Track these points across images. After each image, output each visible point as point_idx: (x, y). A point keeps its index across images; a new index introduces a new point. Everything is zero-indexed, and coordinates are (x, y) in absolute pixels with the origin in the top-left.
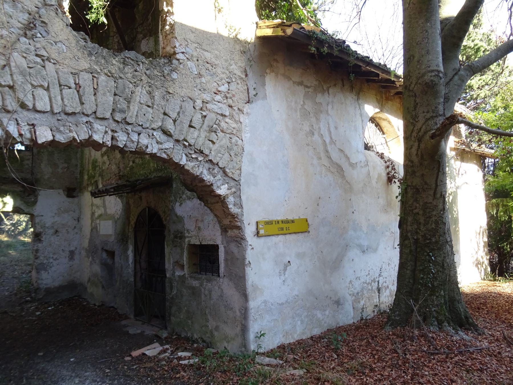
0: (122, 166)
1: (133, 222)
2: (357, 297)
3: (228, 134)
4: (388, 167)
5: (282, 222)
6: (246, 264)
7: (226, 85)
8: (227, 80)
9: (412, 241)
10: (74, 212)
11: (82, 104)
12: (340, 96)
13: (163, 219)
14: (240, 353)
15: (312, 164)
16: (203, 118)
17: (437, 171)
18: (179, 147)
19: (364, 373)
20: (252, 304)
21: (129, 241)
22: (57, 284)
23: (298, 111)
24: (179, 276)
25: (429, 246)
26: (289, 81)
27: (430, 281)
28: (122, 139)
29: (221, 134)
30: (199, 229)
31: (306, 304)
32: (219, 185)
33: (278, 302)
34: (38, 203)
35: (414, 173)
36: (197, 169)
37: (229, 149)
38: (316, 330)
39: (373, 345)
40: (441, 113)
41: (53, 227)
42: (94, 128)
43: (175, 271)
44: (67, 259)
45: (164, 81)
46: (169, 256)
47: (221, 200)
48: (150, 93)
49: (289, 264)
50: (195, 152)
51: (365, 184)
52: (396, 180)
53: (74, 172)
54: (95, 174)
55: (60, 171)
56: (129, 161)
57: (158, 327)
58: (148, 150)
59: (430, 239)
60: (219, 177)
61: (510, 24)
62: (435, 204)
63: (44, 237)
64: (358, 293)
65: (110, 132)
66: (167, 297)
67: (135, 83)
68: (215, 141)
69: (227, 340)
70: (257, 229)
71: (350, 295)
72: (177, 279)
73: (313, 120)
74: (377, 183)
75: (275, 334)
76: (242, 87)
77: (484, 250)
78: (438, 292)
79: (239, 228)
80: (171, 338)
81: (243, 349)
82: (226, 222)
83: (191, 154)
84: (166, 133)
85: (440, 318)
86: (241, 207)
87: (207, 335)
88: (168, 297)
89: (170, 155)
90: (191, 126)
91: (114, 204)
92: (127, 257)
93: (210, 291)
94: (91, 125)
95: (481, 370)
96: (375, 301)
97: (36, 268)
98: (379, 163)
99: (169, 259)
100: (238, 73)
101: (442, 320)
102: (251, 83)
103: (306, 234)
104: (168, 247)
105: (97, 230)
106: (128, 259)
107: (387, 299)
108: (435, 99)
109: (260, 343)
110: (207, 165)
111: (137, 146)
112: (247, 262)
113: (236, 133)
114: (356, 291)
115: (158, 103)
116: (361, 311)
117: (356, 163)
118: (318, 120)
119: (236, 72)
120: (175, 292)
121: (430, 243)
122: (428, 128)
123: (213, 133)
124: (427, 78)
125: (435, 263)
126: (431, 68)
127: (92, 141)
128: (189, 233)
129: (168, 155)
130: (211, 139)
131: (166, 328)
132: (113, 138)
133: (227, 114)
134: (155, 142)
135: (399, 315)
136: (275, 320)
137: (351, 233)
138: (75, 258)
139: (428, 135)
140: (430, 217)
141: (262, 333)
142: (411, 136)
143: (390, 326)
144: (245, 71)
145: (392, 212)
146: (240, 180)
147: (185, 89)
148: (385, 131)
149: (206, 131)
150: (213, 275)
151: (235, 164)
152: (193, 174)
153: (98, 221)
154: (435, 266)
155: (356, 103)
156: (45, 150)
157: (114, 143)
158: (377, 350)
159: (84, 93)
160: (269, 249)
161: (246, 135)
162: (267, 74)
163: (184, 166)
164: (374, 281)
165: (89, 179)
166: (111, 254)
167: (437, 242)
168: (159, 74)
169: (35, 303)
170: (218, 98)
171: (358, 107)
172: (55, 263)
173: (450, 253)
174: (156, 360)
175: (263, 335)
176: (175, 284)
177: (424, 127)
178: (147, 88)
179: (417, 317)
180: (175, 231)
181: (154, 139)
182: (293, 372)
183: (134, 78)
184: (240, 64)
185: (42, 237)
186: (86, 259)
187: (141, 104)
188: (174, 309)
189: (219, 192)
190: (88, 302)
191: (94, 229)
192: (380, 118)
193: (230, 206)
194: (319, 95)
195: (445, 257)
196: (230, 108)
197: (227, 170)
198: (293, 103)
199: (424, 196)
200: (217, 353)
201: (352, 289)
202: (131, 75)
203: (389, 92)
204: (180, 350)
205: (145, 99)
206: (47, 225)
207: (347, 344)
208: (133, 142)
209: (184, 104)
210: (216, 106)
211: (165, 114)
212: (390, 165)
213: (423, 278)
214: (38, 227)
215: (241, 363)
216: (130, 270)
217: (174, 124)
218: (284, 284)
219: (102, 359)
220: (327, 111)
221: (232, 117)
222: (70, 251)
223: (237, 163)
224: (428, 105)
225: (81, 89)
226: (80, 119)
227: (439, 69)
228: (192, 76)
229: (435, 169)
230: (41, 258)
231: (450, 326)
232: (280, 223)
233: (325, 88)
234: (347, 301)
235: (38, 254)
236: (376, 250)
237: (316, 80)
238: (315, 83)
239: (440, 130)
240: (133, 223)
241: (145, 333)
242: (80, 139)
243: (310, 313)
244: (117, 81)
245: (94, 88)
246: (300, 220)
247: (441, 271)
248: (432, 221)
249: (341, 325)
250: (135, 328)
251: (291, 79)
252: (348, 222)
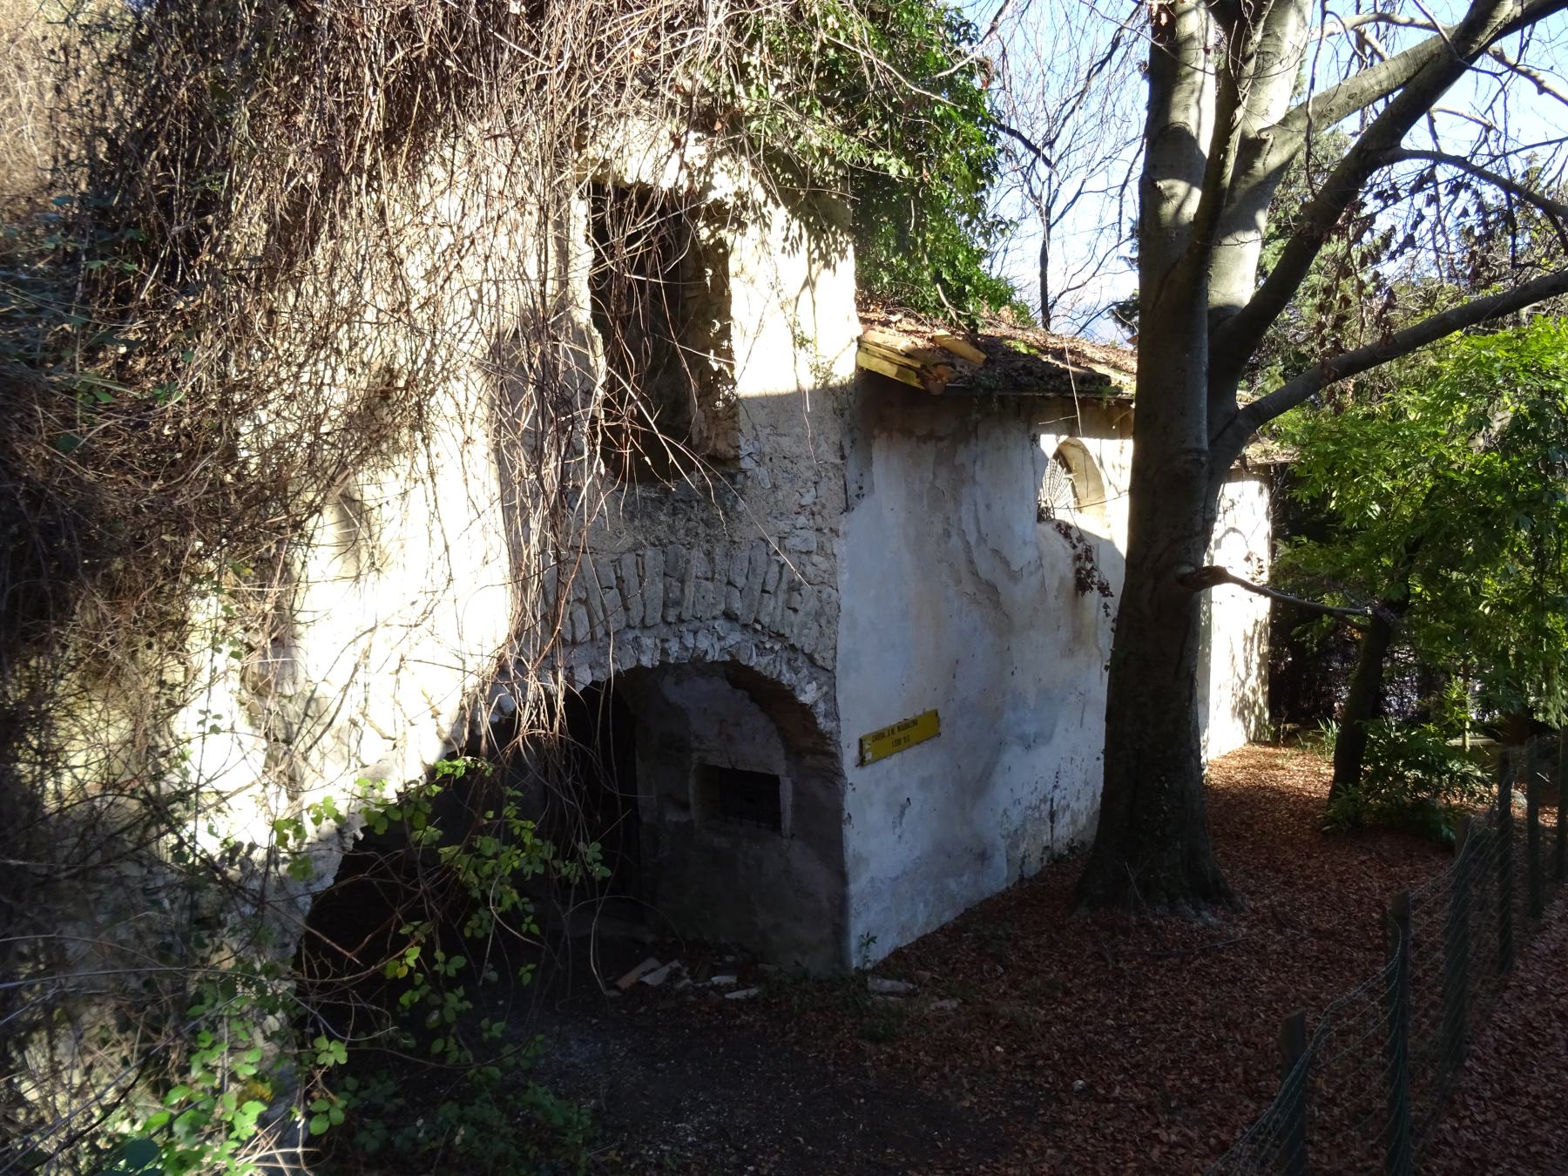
2: (1014, 838)
19: (1055, 1000)
20: (854, 888)
81: (837, 966)
90: (764, 591)
95: (1233, 981)
102: (852, 472)
112: (845, 816)
113: (827, 581)
114: (1012, 829)
126: (1186, 445)
144: (841, 448)
158: (1070, 955)
164: (1044, 801)
175: (873, 940)
182: (941, 1004)
189: (803, 699)
197: (816, 656)
208: (687, 649)
211: (729, 583)
212: (1083, 548)
215: (842, 989)
249: (987, 895)
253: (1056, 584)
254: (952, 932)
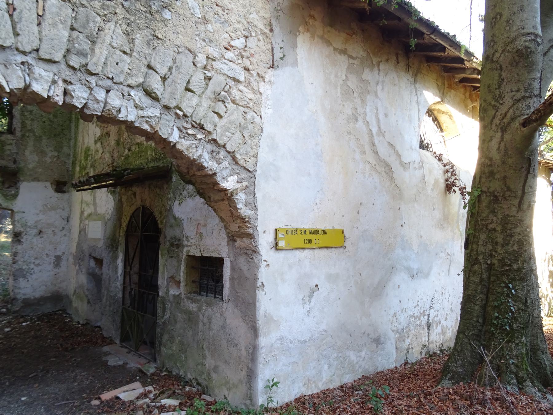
0: (116, 155)
1: (125, 224)
2: (402, 334)
3: (242, 106)
4: (447, 171)
5: (310, 231)
6: (258, 286)
7: (243, 40)
8: (244, 33)
9: (484, 266)
10: (63, 210)
11: (16, 34)
12: (393, 75)
13: (159, 222)
14: (243, 407)
15: (353, 159)
16: (207, 81)
17: (525, 173)
18: (169, 117)
20: (263, 341)
21: (120, 248)
22: (38, 294)
23: (339, 88)
24: (174, 296)
25: (509, 275)
26: (328, 46)
27: (508, 322)
28: (80, 96)
29: (231, 106)
30: (201, 236)
31: (336, 343)
32: (225, 175)
33: (300, 339)
34: (19, 197)
35: (492, 174)
36: (194, 150)
37: (242, 127)
38: (348, 376)
39: (427, 407)
40: (536, 92)
41: (36, 226)
42: (33, 73)
43: (170, 289)
44: (52, 265)
45: (151, 20)
46: (164, 268)
47: (227, 197)
48: (129, 34)
49: (316, 288)
50: (193, 126)
51: (418, 191)
52: (457, 189)
53: (65, 162)
54: (87, 165)
55: (48, 160)
56: (125, 148)
57: (146, 358)
58: (120, 116)
59: (510, 265)
60: (225, 164)
62: (519, 218)
63: (25, 237)
64: (403, 329)
65: (60, 83)
66: (158, 321)
67: (105, 15)
68: (222, 114)
69: (227, 386)
70: (276, 239)
71: (393, 331)
72: (171, 299)
73: (358, 101)
74: (432, 190)
75: (293, 382)
76: (264, 45)
77: (549, 281)
78: (517, 338)
79: (250, 236)
80: (159, 375)
81: (248, 402)
82: (234, 227)
83: (186, 128)
84: (149, 94)
85: (520, 374)
86: (255, 208)
87: (203, 377)
88: (160, 321)
89: (154, 126)
90: (188, 89)
91: (104, 201)
92: (116, 267)
93: (210, 320)
94: (29, 69)
96: (424, 339)
97: (13, 274)
98: (437, 166)
99: (163, 272)
100: (261, 26)
101: (523, 377)
103: (341, 249)
104: (162, 258)
105: (85, 233)
106: (116, 271)
107: (452, 345)
108: (529, 73)
109: (272, 395)
110: (209, 147)
111: (104, 108)
112: (259, 284)
114: (400, 327)
115: (139, 50)
116: (405, 352)
117: (409, 163)
118: (363, 101)
119: (256, 23)
120: (168, 316)
121: (510, 270)
122: (518, 113)
123: (220, 103)
124: (520, 43)
125: (516, 298)
126: (526, 31)
127: (31, 92)
128: (188, 241)
129: (151, 126)
130: (216, 111)
131: (155, 360)
132: (65, 93)
133: (242, 79)
134: (133, 106)
135: (462, 366)
136: (293, 363)
137: (399, 251)
138: (62, 265)
139: (517, 121)
140: (511, 236)
141: (275, 381)
142: (492, 124)
143: (449, 380)
144: (270, 24)
145: (449, 229)
146: (256, 171)
147: (182, 35)
148: (444, 127)
149: (210, 98)
150: (215, 297)
151: (249, 149)
152: (189, 158)
153: (87, 222)
154: (516, 302)
155: (413, 86)
156: (32, 134)
157: (68, 100)
159: (20, 19)
160: (290, 267)
161: (267, 111)
162: (300, 33)
163: (175, 145)
164: (423, 314)
165: (80, 170)
166: (99, 262)
167: (519, 270)
168: (144, 9)
169: (9, 316)
170: (229, 55)
171: (414, 91)
172: (36, 269)
173: (535, 286)
174: (132, 407)
176: (168, 305)
177: (511, 111)
178: (124, 26)
179: (489, 371)
180: (171, 238)
181: (131, 101)
183: (104, 9)
184: (262, 13)
185: (22, 238)
186: (73, 266)
187: (113, 48)
188: (166, 337)
190: (71, 318)
191: (83, 231)
192: (439, 111)
193: (239, 206)
194: (367, 71)
195: (529, 291)
196: (246, 72)
197: (238, 156)
198: (332, 77)
199: (505, 206)
200: (214, 403)
201: (396, 324)
202: (100, 4)
203: (454, 77)
204: (165, 395)
205: (120, 40)
206: (29, 224)
207: (390, 403)
209: (179, 57)
210: (226, 66)
211: (149, 67)
212: (450, 171)
213: (497, 317)
214: (18, 225)
216: (118, 284)
217: (164, 83)
218: (308, 315)
219: (63, 401)
220: (376, 93)
221: (248, 84)
222: (55, 257)
223: (252, 148)
224: (519, 81)
225: (15, 13)
226: (12, 58)
227: (536, 32)
228: (193, 20)
229: (523, 169)
230: (20, 263)
231: (534, 386)
232: (308, 233)
233: (374, 63)
234: (390, 340)
235: (17, 258)
236: (427, 275)
237: (364, 51)
238: (362, 53)
239: (540, 112)
240: (124, 225)
241: (128, 366)
242: (11, 87)
243: (340, 355)
244: (76, 9)
245: (38, 15)
246: (334, 230)
247: (522, 310)
248: (515, 241)
249: (380, 370)
250: (116, 357)
251: (332, 45)
252: (395, 237)
253: (433, 182)
254: (347, 390)
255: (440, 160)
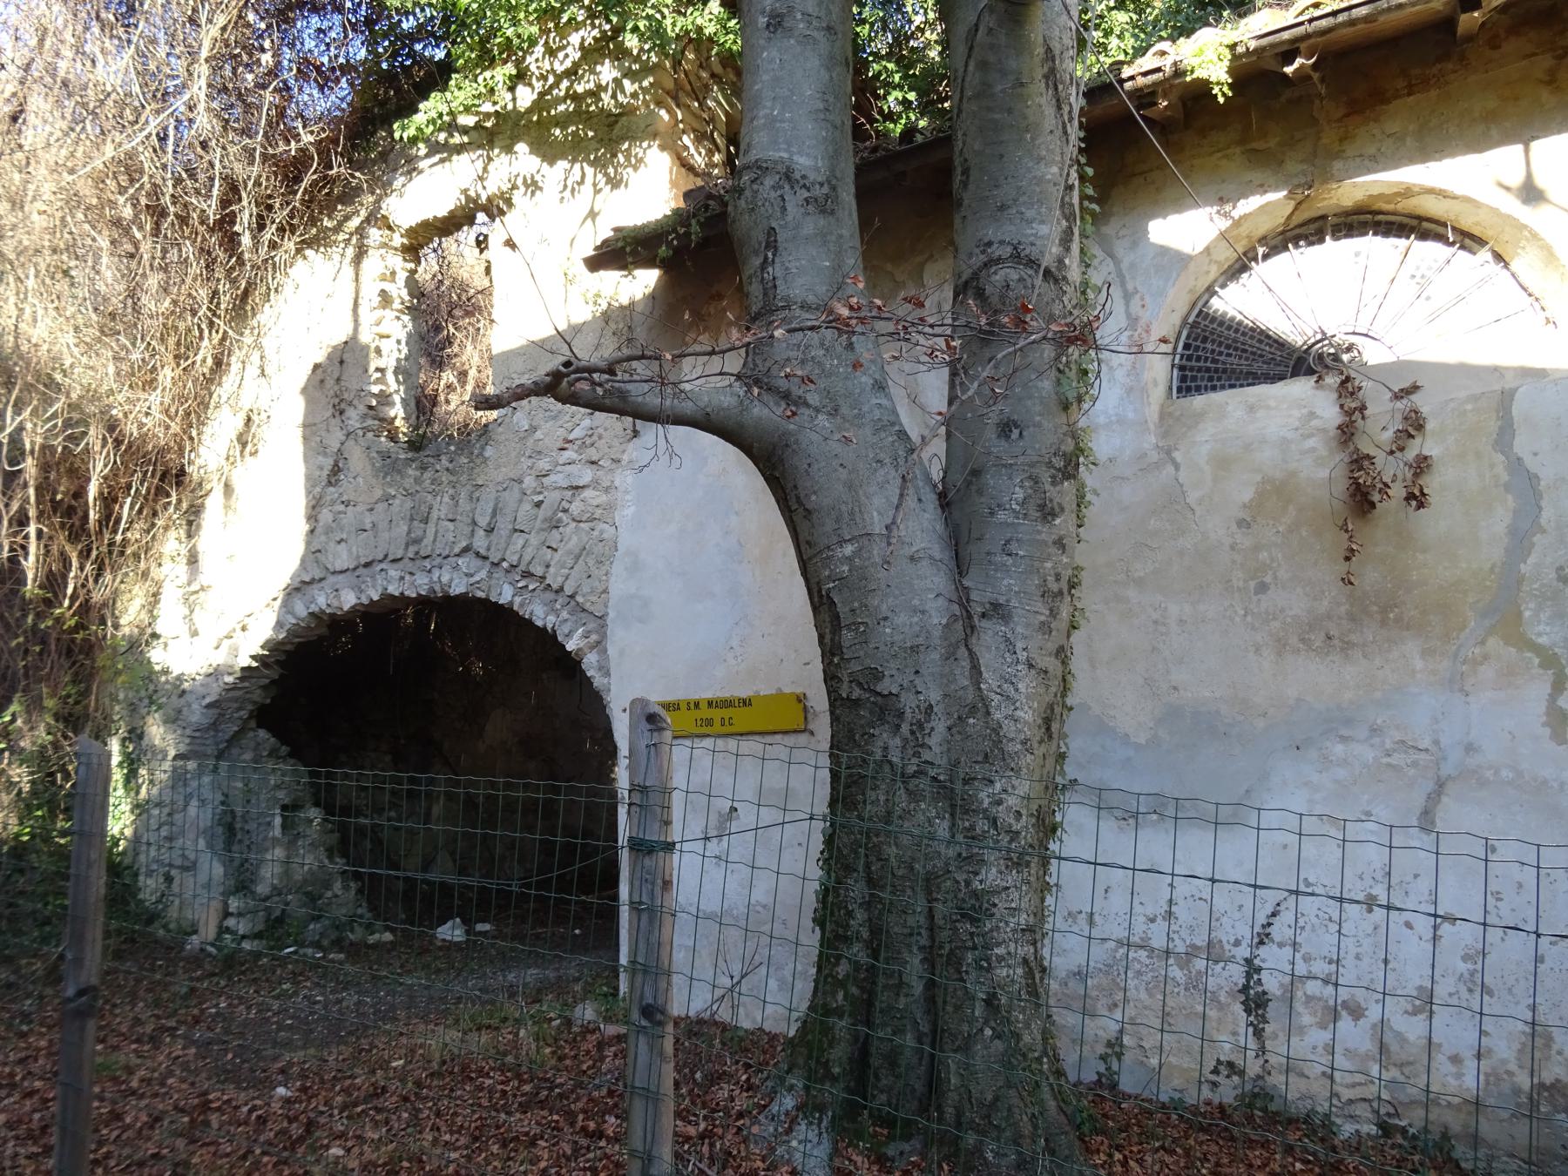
5: (710, 704)
61: (356, 321)
86: (608, 674)
146: (607, 614)
255: (1274, 915)
